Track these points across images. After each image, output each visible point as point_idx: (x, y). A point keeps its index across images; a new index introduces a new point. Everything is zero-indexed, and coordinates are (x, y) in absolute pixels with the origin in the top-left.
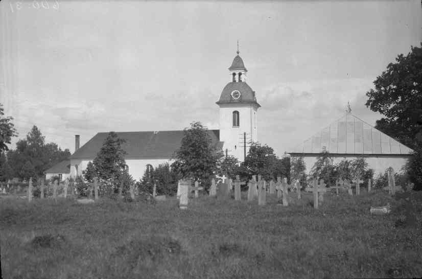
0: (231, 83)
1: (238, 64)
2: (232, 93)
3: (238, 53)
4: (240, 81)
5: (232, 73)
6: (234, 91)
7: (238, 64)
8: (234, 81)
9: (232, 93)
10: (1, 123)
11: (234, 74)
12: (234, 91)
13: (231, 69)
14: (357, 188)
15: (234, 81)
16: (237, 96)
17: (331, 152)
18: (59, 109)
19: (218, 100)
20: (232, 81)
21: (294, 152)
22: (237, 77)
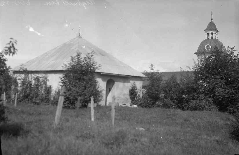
0: (205, 40)
1: (212, 27)
2: (205, 46)
3: (212, 20)
4: (212, 38)
5: (207, 33)
6: (206, 45)
7: (212, 27)
8: (208, 39)
9: (205, 46)
10: (1, 54)
11: (208, 34)
12: (206, 45)
13: (206, 30)
14: (112, 111)
15: (208, 39)
16: (209, 48)
17: (28, 69)
18: (38, 50)
19: (196, 51)
20: (206, 38)
21: (37, 70)
22: (210, 35)
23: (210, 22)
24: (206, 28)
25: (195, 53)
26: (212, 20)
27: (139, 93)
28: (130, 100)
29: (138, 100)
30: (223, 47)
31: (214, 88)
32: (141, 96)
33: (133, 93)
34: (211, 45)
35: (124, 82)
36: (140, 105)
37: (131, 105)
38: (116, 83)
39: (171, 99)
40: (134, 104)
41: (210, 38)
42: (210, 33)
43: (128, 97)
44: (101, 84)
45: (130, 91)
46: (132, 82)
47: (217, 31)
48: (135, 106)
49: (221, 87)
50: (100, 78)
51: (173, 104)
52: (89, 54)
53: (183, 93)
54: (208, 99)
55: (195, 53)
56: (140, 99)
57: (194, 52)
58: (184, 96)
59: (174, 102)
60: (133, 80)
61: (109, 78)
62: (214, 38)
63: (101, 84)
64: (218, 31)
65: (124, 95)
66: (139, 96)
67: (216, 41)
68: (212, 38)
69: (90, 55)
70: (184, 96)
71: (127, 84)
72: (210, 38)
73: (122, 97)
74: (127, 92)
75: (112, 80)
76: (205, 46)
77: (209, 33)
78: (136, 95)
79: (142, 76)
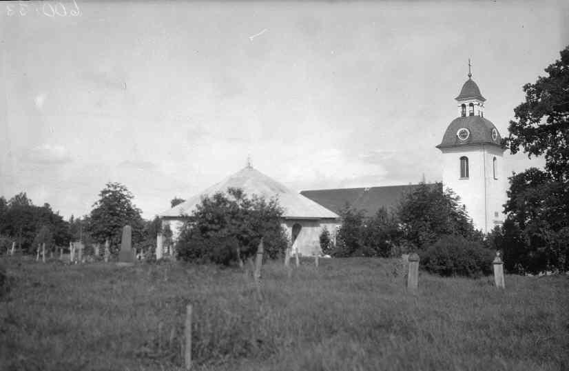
1: (470, 91)
3: (470, 76)
4: (472, 114)
5: (460, 105)
7: (470, 91)
8: (464, 115)
11: (464, 106)
15: (464, 115)
16: (464, 136)
19: (439, 142)
22: (468, 109)
23: (466, 80)
24: (458, 94)
25: (437, 147)
26: (470, 76)
27: (332, 240)
28: (321, 250)
29: (331, 249)
30: (494, 133)
31: (417, 233)
32: (335, 243)
33: (324, 239)
34: (469, 130)
35: (313, 226)
36: (335, 254)
37: (323, 256)
38: (303, 228)
39: (373, 245)
40: (326, 254)
41: (468, 115)
42: (467, 103)
43: (319, 245)
44: (288, 230)
45: (320, 238)
46: (322, 225)
47: (482, 99)
48: (328, 256)
49: (426, 230)
50: (284, 222)
51: (375, 252)
52: (273, 197)
53: (386, 238)
54: (412, 244)
55: (437, 147)
56: (333, 247)
57: (437, 145)
58: (387, 242)
59: (376, 249)
60: (323, 223)
61: (294, 223)
62: (475, 114)
63: (288, 230)
64: (482, 99)
65: (314, 242)
66: (333, 243)
67: (480, 120)
68: (472, 114)
69: (275, 199)
70: (387, 242)
71: (316, 229)
72: (468, 115)
73: (311, 245)
74: (317, 239)
75: (298, 225)
76: (460, 128)
77: (466, 104)
78: (328, 242)
79: (333, 217)
